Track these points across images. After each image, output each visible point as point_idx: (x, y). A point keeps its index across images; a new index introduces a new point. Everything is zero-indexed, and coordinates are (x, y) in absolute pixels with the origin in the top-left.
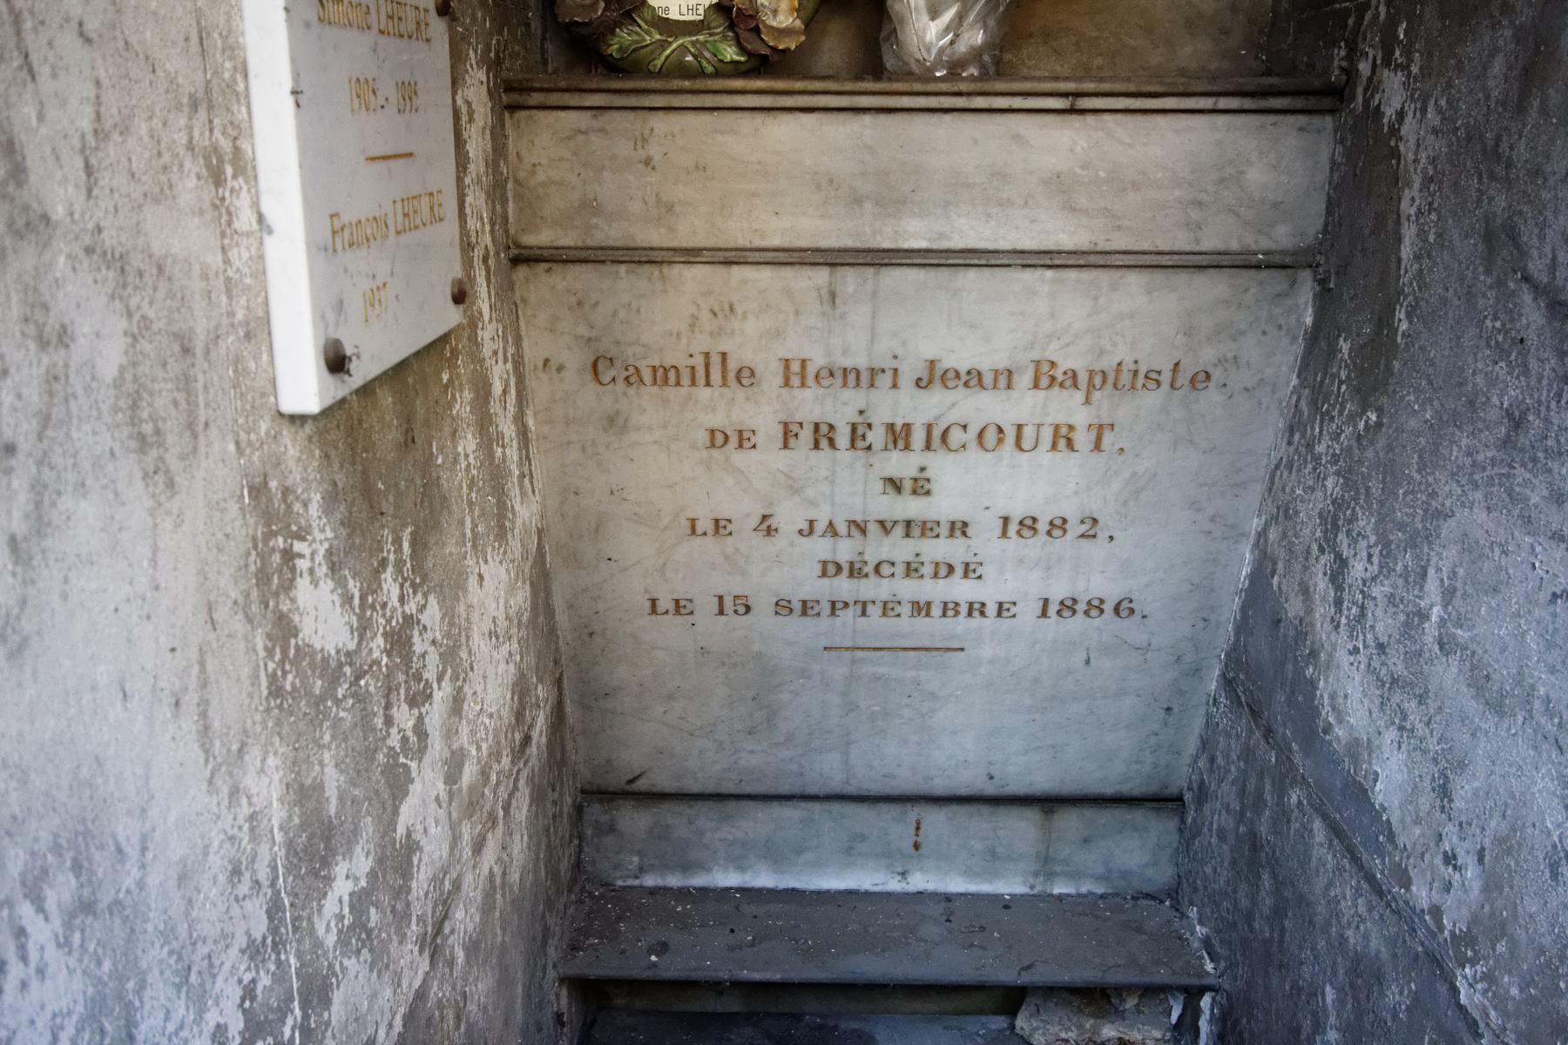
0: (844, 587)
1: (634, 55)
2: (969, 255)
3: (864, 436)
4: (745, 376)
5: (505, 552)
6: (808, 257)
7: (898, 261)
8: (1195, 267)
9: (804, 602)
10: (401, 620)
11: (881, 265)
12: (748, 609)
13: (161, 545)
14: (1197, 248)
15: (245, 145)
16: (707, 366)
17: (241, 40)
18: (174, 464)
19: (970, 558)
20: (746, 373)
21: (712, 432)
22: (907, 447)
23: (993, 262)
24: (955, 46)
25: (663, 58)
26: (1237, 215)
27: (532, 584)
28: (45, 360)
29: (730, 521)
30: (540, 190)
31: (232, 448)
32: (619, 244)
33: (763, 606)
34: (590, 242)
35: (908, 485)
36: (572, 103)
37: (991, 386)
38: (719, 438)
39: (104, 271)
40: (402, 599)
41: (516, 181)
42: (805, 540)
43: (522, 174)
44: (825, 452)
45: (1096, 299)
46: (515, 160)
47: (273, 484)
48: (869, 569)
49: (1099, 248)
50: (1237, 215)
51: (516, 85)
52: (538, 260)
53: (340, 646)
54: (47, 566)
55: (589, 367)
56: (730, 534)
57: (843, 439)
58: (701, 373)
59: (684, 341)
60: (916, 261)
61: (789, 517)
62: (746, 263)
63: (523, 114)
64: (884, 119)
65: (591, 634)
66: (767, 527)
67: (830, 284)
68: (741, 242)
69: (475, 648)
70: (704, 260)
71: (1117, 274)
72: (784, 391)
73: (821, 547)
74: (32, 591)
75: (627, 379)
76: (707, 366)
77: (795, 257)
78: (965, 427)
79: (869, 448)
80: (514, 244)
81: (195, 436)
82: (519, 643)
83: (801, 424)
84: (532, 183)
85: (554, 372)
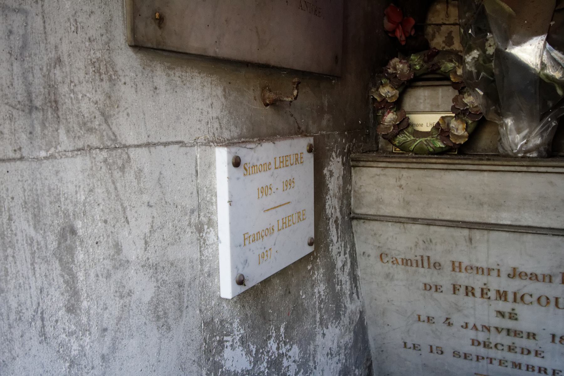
0: (481, 351)
1: (404, 144)
3: (487, 294)
4: (437, 266)
5: (339, 323)
9: (465, 354)
10: (277, 356)
11: (490, 230)
12: (442, 353)
13: (162, 348)
15: (213, 217)
16: (422, 260)
17: (215, 186)
18: (171, 321)
19: (538, 349)
20: (437, 265)
21: (425, 284)
22: (506, 300)
23: (539, 232)
25: (414, 146)
27: (355, 332)
28: (122, 301)
29: (433, 318)
30: (362, 195)
31: (198, 312)
32: (388, 215)
33: (448, 353)
34: (379, 213)
35: (507, 315)
36: (374, 166)
37: (542, 280)
38: (428, 287)
39: (148, 271)
40: (278, 349)
41: (354, 191)
42: (464, 330)
43: (356, 189)
44: (470, 298)
47: (216, 320)
48: (492, 345)
52: (361, 219)
53: (244, 368)
54: (115, 361)
55: (379, 255)
56: (434, 323)
57: (478, 293)
58: (420, 262)
59: (413, 251)
60: (504, 229)
61: (457, 319)
63: (358, 168)
64: (492, 174)
65: (382, 351)
66: (448, 322)
67: (469, 235)
68: (435, 217)
69: (317, 360)
72: (453, 273)
73: (472, 334)
74: (108, 370)
75: (393, 262)
76: (422, 260)
77: (455, 224)
78: (531, 295)
79: (489, 298)
81: (182, 312)
82: (345, 355)
83: (460, 286)
85: (367, 257)
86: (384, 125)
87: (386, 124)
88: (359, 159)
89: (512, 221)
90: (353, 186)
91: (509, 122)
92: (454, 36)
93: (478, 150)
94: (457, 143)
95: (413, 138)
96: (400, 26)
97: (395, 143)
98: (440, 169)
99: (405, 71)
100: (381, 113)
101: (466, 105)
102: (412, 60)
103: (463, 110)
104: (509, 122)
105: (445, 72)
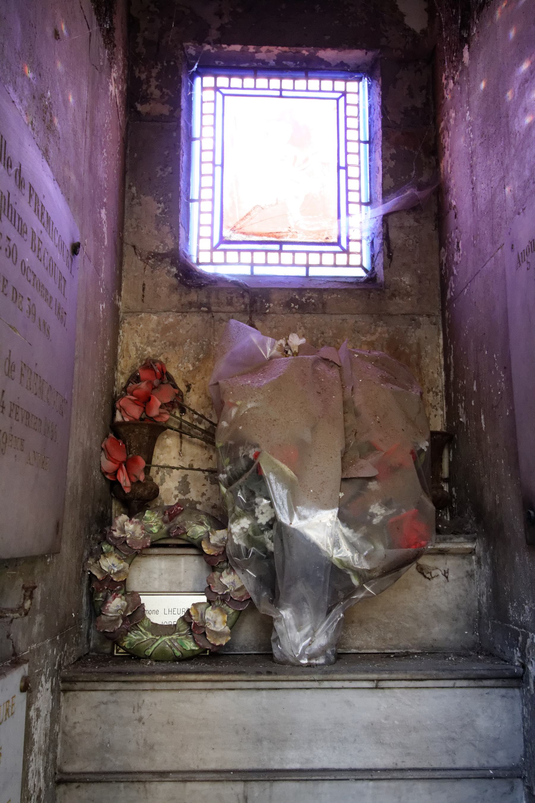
2: (324, 774)
6: (231, 775)
7: (284, 778)
8: (455, 778)
11: (274, 781)
14: (454, 766)
23: (338, 778)
24: (312, 646)
26: (475, 746)
36: (100, 688)
41: (64, 732)
43: (67, 729)
45: (400, 798)
46: (65, 719)
49: (399, 767)
50: (475, 746)
51: (68, 679)
60: (293, 778)
62: (194, 781)
67: (244, 792)
68: (193, 767)
70: (170, 780)
71: (411, 783)
80: (59, 771)
84: (73, 733)
86: (107, 616)
87: (111, 615)
88: (76, 679)
89: (301, 763)
90: (61, 724)
91: (286, 614)
92: (190, 482)
93: (235, 648)
94: (217, 644)
95: (150, 636)
96: (124, 467)
97: (124, 645)
98: (200, 689)
99: (137, 535)
100: (102, 597)
101: (225, 587)
102: (146, 519)
103: (222, 595)
104: (286, 614)
105: (193, 538)
